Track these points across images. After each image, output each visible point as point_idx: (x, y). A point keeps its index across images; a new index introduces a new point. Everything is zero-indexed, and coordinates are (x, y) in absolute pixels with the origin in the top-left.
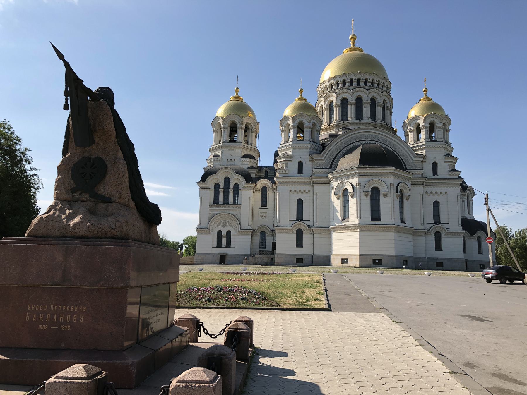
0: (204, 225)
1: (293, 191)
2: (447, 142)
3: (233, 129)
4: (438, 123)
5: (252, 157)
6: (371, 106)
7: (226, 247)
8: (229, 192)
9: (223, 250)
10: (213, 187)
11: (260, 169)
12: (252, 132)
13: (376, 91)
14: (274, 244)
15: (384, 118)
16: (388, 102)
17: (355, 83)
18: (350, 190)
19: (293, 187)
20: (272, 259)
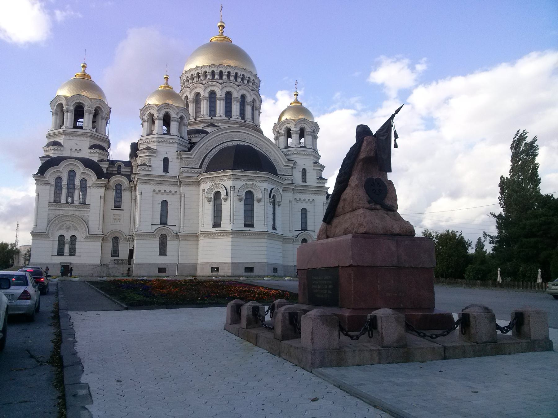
0: (42, 228)
1: (157, 191)
2: (315, 150)
3: (79, 112)
4: (308, 130)
5: (103, 148)
6: (240, 103)
7: (70, 255)
8: (61, 188)
9: (66, 259)
10: (53, 181)
11: (112, 163)
12: (102, 118)
13: (246, 88)
14: (131, 252)
15: (253, 118)
16: (257, 101)
17: (224, 77)
18: (223, 194)
19: (157, 188)
20: (129, 268)
